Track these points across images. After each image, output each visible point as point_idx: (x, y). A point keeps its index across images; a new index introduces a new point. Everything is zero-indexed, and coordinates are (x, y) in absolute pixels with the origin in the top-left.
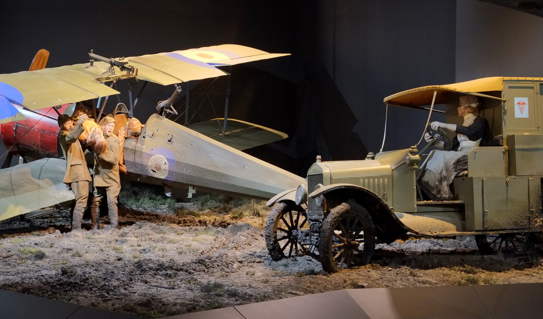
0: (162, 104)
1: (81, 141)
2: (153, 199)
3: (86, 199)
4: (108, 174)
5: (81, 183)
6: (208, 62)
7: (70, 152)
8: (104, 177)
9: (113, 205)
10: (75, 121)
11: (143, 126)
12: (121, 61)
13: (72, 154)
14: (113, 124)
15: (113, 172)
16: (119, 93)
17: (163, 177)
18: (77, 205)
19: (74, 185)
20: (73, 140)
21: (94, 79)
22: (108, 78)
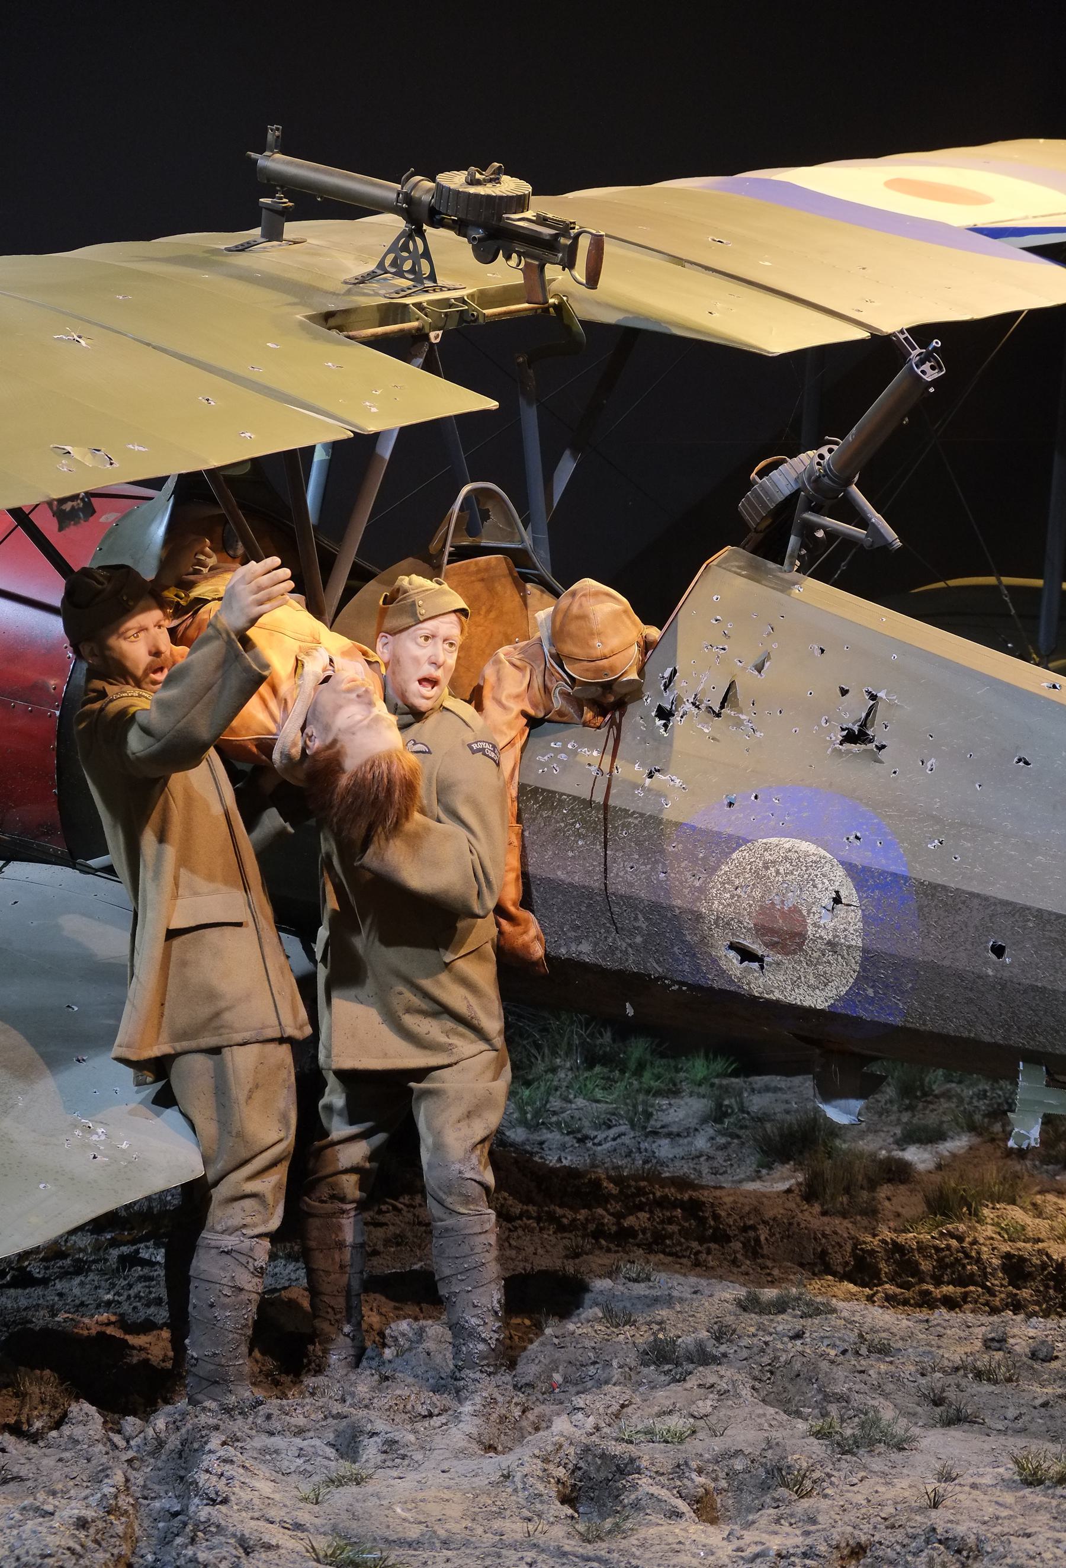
0: (789, 474)
1: (231, 755)
2: (607, 1060)
3: (279, 1176)
4: (427, 984)
5: (243, 1061)
6: (970, 223)
7: (162, 838)
8: (398, 1007)
9: (467, 1200)
10: (179, 611)
11: (654, 633)
12: (472, 190)
13: (170, 852)
14: (449, 626)
15: (462, 965)
16: (493, 404)
17: (818, 1000)
18: (220, 1216)
19: (194, 1076)
20: (183, 753)
21: (300, 315)
22: (393, 312)
